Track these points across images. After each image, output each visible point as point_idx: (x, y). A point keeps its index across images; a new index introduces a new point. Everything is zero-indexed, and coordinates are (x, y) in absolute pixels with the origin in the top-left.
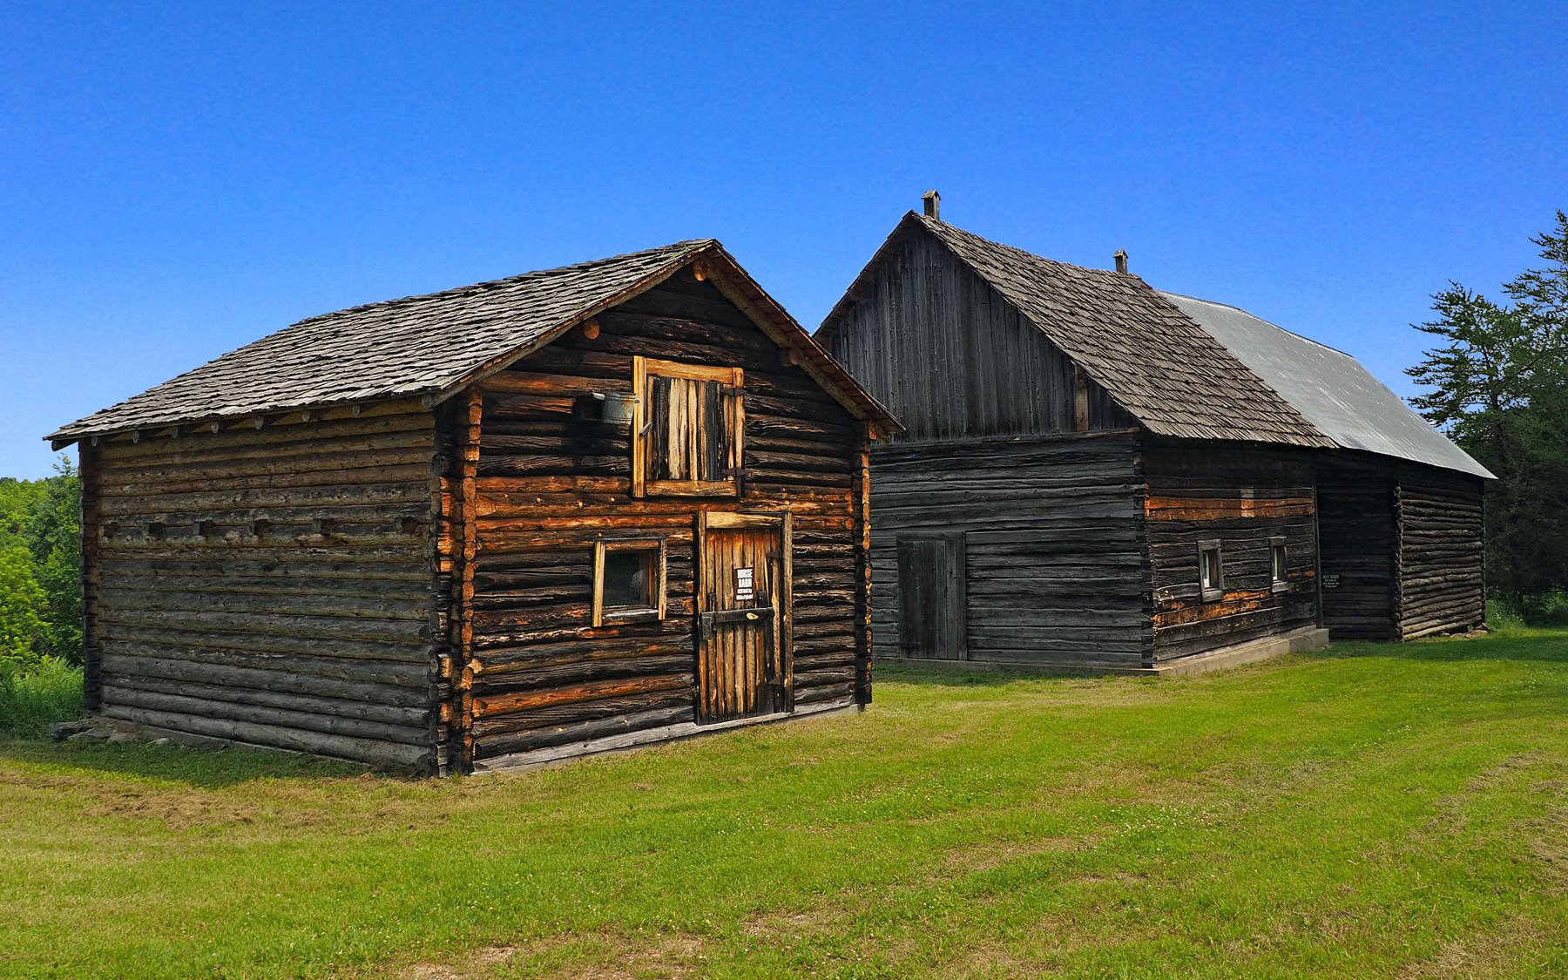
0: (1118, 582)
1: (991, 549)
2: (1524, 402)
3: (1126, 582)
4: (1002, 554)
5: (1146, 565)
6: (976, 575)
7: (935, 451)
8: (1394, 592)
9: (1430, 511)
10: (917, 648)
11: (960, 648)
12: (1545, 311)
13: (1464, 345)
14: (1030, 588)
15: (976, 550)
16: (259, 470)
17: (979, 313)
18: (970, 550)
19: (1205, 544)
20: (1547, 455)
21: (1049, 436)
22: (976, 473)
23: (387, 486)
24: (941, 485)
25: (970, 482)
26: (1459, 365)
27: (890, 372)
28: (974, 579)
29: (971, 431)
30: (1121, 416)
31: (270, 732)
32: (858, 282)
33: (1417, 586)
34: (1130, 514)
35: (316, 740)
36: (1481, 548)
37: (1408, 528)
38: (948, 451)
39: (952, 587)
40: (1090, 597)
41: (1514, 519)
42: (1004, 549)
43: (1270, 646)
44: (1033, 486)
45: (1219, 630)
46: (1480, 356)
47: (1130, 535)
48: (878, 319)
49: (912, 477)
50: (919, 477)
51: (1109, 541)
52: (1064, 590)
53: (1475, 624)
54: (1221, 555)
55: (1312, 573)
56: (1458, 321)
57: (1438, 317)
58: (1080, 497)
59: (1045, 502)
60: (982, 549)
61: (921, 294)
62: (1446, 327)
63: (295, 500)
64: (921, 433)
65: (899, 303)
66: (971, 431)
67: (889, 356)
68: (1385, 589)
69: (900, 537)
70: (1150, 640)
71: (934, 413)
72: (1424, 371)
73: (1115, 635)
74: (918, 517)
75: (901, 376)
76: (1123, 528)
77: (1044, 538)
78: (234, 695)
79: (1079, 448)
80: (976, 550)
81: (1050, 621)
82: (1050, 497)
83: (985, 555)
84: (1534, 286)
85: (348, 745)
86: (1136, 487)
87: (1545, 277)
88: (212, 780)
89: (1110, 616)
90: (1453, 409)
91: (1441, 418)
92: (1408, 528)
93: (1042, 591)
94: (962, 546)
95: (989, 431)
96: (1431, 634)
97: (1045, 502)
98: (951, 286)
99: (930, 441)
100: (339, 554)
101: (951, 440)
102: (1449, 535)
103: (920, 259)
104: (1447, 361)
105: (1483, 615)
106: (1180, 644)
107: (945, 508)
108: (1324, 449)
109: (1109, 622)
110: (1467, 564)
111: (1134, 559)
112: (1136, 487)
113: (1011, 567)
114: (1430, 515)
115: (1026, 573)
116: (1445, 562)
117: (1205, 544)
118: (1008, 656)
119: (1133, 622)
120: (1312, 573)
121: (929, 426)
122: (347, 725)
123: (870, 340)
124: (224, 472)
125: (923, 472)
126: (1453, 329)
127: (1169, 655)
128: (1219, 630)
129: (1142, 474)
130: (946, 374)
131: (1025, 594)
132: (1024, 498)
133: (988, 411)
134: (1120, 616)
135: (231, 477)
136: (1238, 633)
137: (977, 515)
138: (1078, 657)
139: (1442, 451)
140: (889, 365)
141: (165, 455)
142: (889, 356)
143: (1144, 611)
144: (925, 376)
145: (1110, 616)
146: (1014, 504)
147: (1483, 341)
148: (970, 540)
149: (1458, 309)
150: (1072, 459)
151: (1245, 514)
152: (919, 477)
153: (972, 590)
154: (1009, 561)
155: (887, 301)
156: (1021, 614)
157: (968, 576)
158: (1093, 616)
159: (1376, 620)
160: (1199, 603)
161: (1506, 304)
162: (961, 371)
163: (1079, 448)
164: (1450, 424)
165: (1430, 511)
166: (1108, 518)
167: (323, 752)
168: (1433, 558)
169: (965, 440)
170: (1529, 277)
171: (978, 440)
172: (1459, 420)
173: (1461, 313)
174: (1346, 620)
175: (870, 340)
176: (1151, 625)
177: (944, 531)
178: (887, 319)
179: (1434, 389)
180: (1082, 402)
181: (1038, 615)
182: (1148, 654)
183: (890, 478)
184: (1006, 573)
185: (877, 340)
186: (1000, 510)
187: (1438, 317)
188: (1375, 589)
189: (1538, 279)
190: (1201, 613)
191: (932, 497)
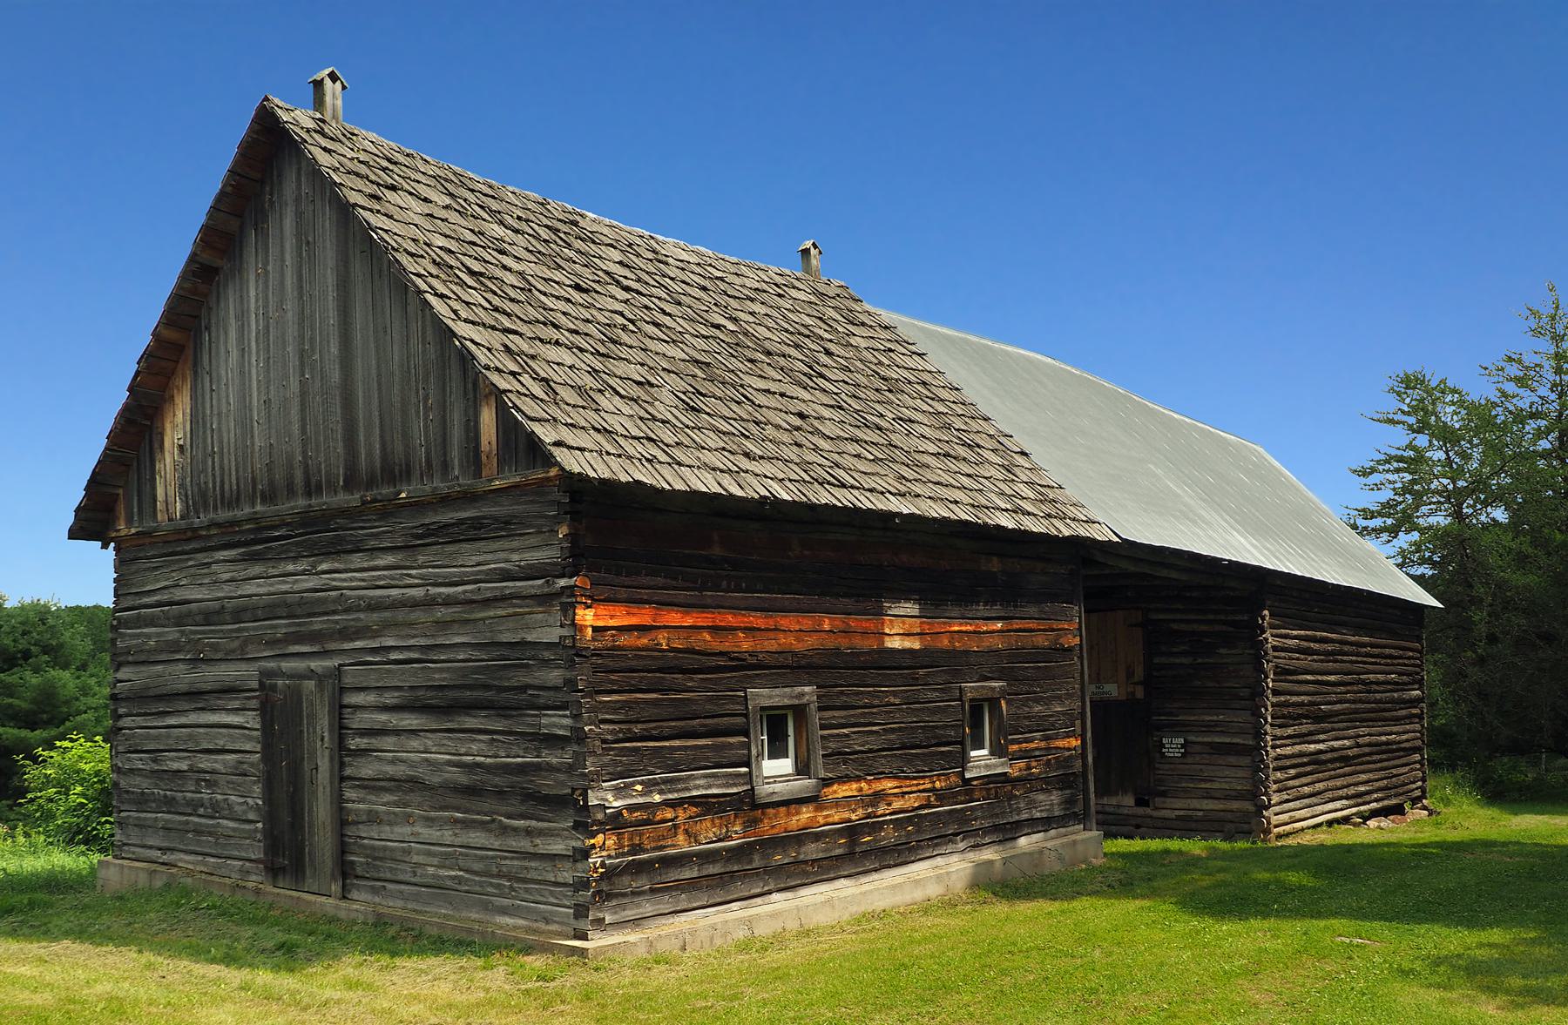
0: (537, 768)
2: (1500, 515)
3: (551, 768)
4: (386, 708)
5: (579, 737)
8: (1258, 766)
9: (1329, 647)
10: (283, 869)
11: (333, 878)
12: (1528, 401)
13: (1422, 440)
14: (420, 772)
17: (358, 269)
19: (764, 696)
20: (1519, 579)
21: (441, 486)
22: (357, 560)
24: (312, 582)
25: (348, 577)
26: (1414, 461)
30: (536, 452)
32: (207, 231)
33: (1301, 755)
34: (553, 635)
36: (1419, 700)
37: (1281, 672)
39: (324, 764)
40: (500, 794)
41: (1481, 661)
43: (944, 872)
44: (428, 582)
45: (812, 851)
46: (1441, 455)
47: (554, 676)
48: (242, 299)
50: (291, 568)
51: (524, 688)
52: (463, 779)
53: (1415, 801)
54: (815, 718)
55: (1075, 742)
56: (1414, 411)
57: (1391, 404)
58: (487, 603)
61: (290, 244)
62: (1399, 417)
64: (291, 491)
65: (266, 263)
66: (349, 485)
67: (254, 359)
68: (1246, 761)
69: (265, 674)
70: (583, 884)
72: (1373, 470)
73: (536, 869)
76: (546, 663)
77: (439, 678)
79: (487, 510)
81: (447, 835)
83: (366, 711)
84: (1513, 370)
86: (562, 582)
87: (1529, 359)
89: (529, 832)
90: (1405, 522)
91: (1394, 531)
92: (1281, 672)
93: (436, 780)
94: (336, 686)
95: (371, 483)
96: (1330, 823)
97: (441, 613)
101: (326, 500)
102: (1363, 682)
104: (1400, 459)
105: (1424, 792)
106: (692, 885)
107: (318, 623)
108: (1078, 545)
109: (524, 844)
110: (1398, 720)
111: (558, 722)
112: (562, 582)
113: (397, 732)
114: (1332, 653)
115: (415, 743)
116: (1353, 718)
117: (764, 696)
118: (392, 895)
119: (558, 847)
120: (1075, 742)
123: (233, 334)
126: (1412, 420)
127: (648, 908)
128: (812, 851)
129: (577, 558)
130: (318, 384)
131: (413, 781)
132: (415, 604)
133: (370, 449)
134: (541, 833)
136: (860, 850)
138: (486, 907)
139: (1384, 572)
140: (254, 371)
142: (254, 359)
143: (578, 826)
144: (294, 386)
145: (529, 832)
146: (401, 615)
147: (1447, 436)
148: (348, 681)
149: (1416, 394)
150: (474, 532)
151: (895, 643)
152: (291, 568)
153: (348, 772)
155: (253, 259)
156: (407, 819)
157: (341, 739)
158: (505, 830)
159: (1235, 805)
160: (749, 805)
161: (1481, 390)
162: (335, 376)
163: (487, 510)
164: (1405, 540)
165: (1329, 647)
166: (523, 644)
168: (1338, 713)
170: (1510, 359)
172: (1415, 536)
173: (1420, 399)
174: (1195, 803)
176: (585, 853)
177: (315, 664)
178: (252, 293)
179: (1386, 495)
180: (488, 418)
181: (430, 822)
182: (581, 911)
184: (388, 742)
186: (386, 626)
187: (1391, 404)
188: (1232, 760)
189: (1520, 362)
190: (753, 823)
191: (302, 603)
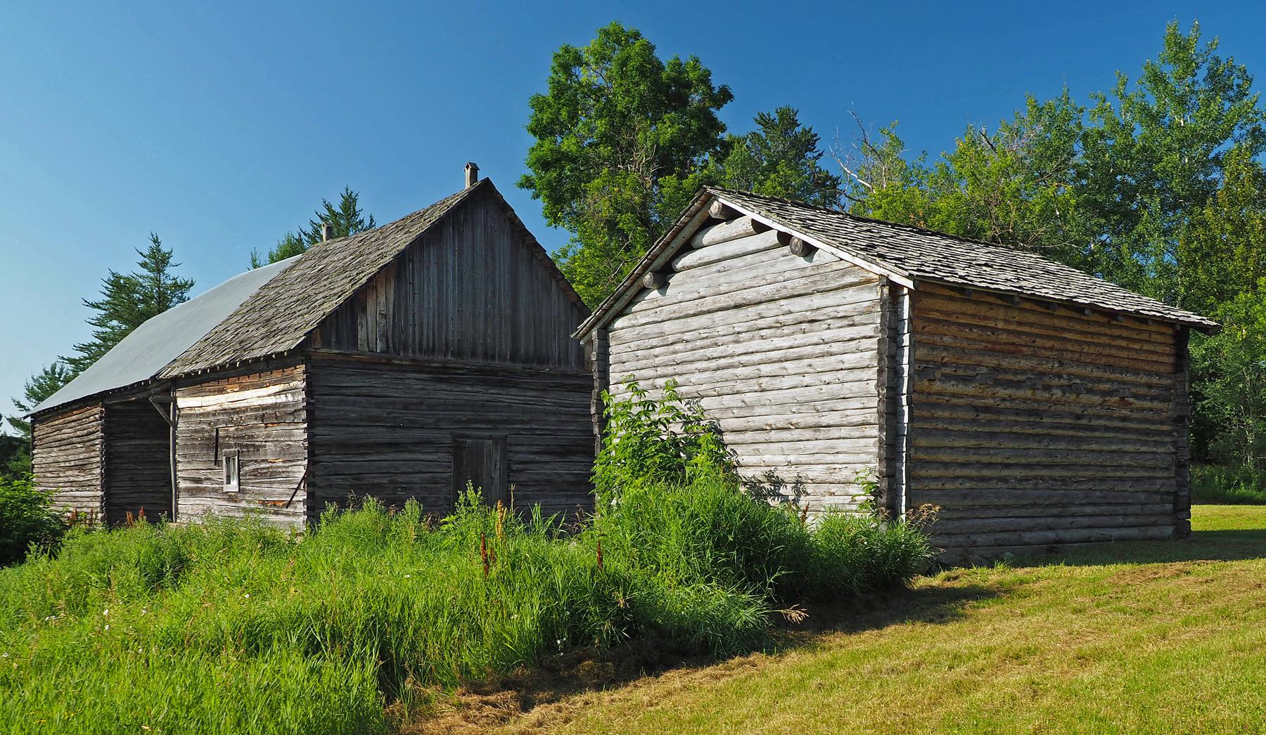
1: (524, 448)
6: (515, 467)
7: (480, 371)
15: (515, 448)
16: (1077, 348)
18: (510, 448)
22: (514, 391)
23: (1149, 374)
24: (486, 397)
25: (510, 396)
27: (451, 301)
28: (513, 471)
29: (514, 358)
31: (1084, 533)
35: (1116, 533)
38: (493, 372)
42: (535, 449)
49: (462, 388)
50: (469, 389)
59: (563, 418)
60: (519, 448)
63: (1096, 373)
64: (474, 354)
65: (461, 245)
66: (514, 358)
71: (485, 340)
74: (469, 421)
75: (460, 305)
78: (1055, 511)
80: (515, 448)
82: (567, 414)
85: (1133, 532)
88: (974, 587)
95: (527, 361)
98: (503, 243)
99: (480, 362)
100: (1125, 412)
101: (497, 363)
103: (480, 216)
107: (491, 416)
121: (480, 349)
122: (1131, 520)
124: (1049, 344)
125: (472, 386)
135: (1051, 349)
137: (515, 422)
141: (986, 318)
142: (451, 288)
154: (537, 458)
167: (1121, 539)
169: (508, 364)
171: (519, 366)
175: (433, 270)
178: (450, 256)
183: (443, 386)
185: (440, 272)
